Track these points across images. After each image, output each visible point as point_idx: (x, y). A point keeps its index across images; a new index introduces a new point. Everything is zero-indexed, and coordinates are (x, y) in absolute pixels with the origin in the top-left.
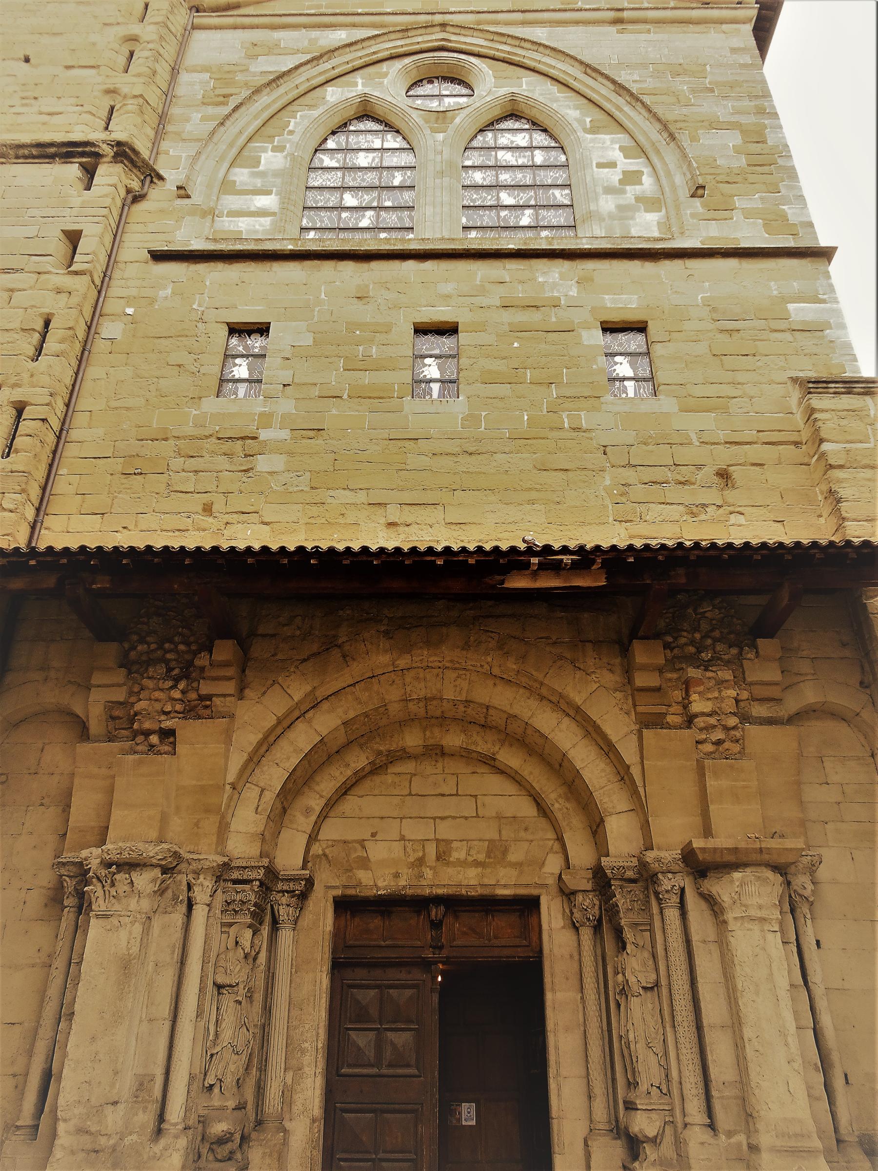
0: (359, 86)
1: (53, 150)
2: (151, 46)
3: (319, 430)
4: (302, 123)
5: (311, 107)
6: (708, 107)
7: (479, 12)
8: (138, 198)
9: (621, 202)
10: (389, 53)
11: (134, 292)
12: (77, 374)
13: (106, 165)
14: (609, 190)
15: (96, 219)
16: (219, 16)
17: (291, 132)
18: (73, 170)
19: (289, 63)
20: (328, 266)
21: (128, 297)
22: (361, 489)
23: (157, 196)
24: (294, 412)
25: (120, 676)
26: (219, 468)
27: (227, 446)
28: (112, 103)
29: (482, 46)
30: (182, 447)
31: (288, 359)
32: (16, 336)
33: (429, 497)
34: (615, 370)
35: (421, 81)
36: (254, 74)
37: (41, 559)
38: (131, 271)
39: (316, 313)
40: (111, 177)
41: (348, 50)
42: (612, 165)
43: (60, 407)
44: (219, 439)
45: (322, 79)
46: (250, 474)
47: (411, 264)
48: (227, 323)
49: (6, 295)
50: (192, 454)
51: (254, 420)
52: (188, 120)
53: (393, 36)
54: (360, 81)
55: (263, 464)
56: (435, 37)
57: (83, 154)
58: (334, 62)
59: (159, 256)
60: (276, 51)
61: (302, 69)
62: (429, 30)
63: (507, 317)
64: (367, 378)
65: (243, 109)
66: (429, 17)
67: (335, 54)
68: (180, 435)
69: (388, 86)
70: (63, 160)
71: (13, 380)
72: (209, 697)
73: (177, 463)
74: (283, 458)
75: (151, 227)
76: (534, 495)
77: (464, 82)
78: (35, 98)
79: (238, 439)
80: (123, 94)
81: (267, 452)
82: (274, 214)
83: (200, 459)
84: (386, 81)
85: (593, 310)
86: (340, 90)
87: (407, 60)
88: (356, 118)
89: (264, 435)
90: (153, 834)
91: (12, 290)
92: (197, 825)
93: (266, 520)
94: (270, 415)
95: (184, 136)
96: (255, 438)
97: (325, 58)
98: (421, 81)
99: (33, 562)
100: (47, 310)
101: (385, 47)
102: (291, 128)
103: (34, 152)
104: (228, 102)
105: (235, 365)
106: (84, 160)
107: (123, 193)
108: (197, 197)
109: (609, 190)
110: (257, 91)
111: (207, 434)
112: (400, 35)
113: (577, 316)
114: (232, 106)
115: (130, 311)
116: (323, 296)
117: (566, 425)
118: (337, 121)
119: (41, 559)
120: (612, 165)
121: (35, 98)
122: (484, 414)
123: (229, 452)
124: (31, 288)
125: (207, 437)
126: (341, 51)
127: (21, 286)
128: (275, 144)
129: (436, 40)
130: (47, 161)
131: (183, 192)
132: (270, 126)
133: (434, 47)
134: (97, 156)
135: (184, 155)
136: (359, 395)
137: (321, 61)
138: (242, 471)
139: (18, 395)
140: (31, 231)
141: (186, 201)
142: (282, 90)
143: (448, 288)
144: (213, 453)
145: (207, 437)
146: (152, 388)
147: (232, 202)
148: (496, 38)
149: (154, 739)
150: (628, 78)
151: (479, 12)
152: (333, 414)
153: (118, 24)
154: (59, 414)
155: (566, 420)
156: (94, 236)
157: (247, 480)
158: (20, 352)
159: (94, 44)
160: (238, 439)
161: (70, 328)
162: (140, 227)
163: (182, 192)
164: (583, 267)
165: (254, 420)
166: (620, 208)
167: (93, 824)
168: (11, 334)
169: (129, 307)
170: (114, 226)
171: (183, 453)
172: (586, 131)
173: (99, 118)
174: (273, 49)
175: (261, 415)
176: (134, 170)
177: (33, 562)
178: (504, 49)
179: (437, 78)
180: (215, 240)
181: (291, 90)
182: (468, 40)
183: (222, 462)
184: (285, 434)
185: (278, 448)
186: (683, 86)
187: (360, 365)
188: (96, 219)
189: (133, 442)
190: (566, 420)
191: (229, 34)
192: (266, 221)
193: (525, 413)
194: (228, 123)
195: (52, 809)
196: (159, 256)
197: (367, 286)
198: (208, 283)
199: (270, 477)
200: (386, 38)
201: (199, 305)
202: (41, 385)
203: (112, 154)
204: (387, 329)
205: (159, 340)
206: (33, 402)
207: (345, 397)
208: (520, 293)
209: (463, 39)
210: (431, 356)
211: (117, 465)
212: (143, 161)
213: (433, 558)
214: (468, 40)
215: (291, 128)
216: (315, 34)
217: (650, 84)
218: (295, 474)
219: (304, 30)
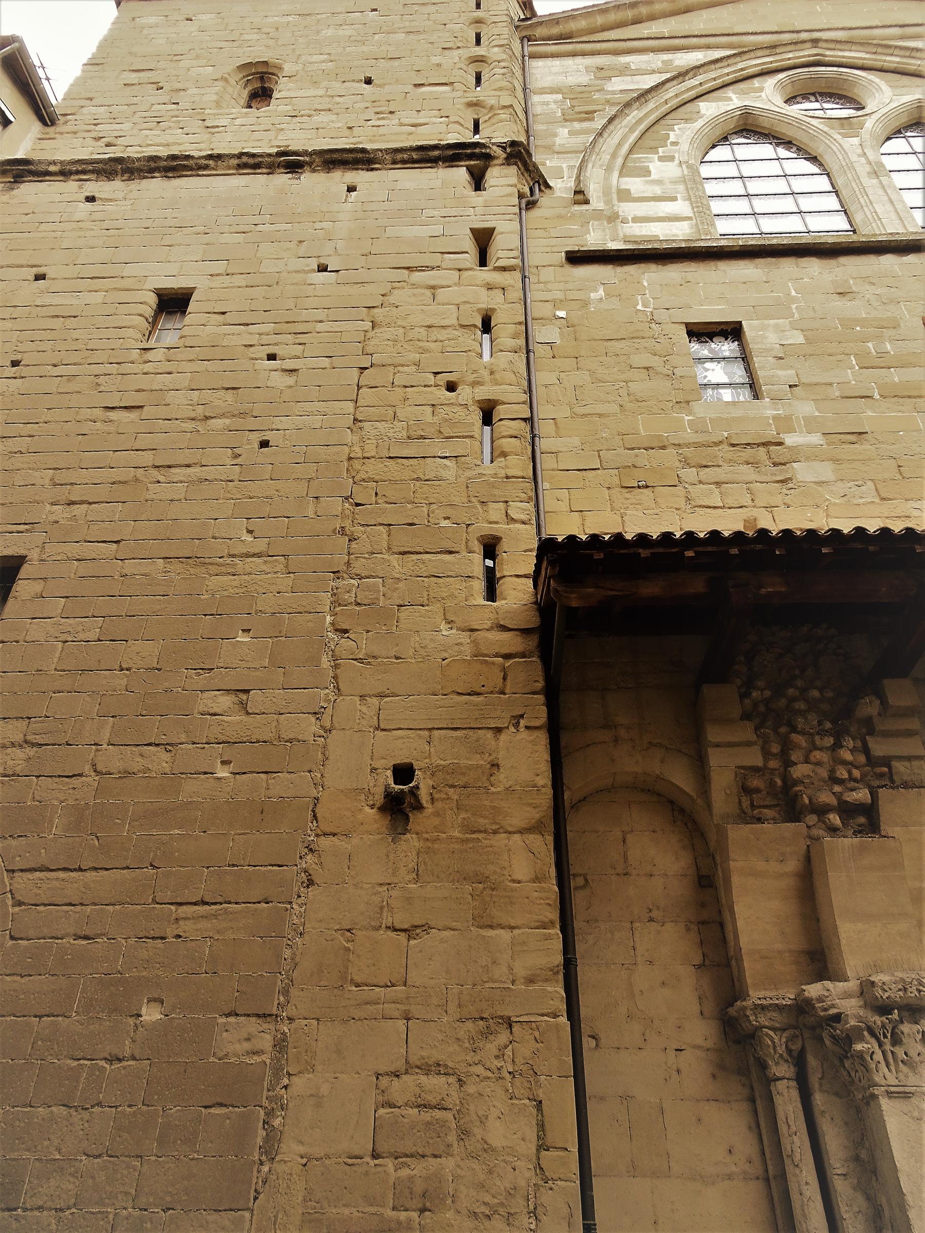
0: (735, 100)
1: (436, 153)
2: (503, 64)
3: (860, 433)
4: (683, 135)
7: (850, 29)
8: (531, 205)
10: (760, 68)
11: (559, 295)
13: (497, 167)
15: (508, 217)
16: (556, 44)
17: (675, 144)
18: (460, 174)
19: (648, 82)
20: (788, 265)
21: (554, 301)
24: (817, 414)
25: (746, 732)
26: (747, 479)
27: (748, 453)
28: (476, 117)
29: (864, 59)
30: (689, 455)
31: (781, 358)
35: (795, 97)
36: (614, 92)
37: (701, 549)
38: (547, 274)
39: (794, 311)
40: (503, 180)
41: (713, 67)
44: (733, 445)
45: (693, 93)
46: (790, 485)
47: (889, 260)
48: (687, 325)
49: (428, 293)
50: (705, 463)
52: (555, 135)
53: (760, 53)
54: (733, 96)
56: (807, 53)
57: (471, 157)
58: (700, 79)
59: (576, 258)
62: (799, 46)
64: (895, 376)
65: (616, 121)
66: (795, 36)
67: (701, 71)
68: (681, 442)
69: (767, 97)
70: (447, 164)
71: (471, 378)
72: (886, 761)
73: (689, 474)
75: (554, 233)
77: (845, 97)
78: (391, 113)
79: (758, 445)
80: (489, 106)
81: (802, 460)
82: (689, 218)
83: (716, 469)
84: (763, 94)
86: (714, 104)
88: (735, 133)
89: (790, 440)
94: (788, 418)
95: (557, 148)
97: (691, 74)
98: (795, 97)
99: (690, 554)
100: (484, 306)
101: (753, 64)
103: (415, 156)
105: (707, 370)
106: (472, 163)
108: (597, 203)
110: (628, 105)
111: (715, 440)
112: (767, 52)
116: (793, 293)
118: (718, 133)
119: (701, 549)
121: (391, 113)
123: (751, 460)
124: (455, 284)
125: (717, 444)
126: (706, 68)
127: (444, 283)
128: (661, 154)
129: (809, 56)
130: (429, 165)
132: (650, 137)
133: (808, 61)
134: (488, 158)
135: (564, 166)
137: (687, 78)
138: (778, 482)
139: (485, 392)
140: (438, 230)
141: (585, 207)
142: (651, 105)
145: (717, 444)
146: (623, 392)
147: (628, 209)
148: (879, 50)
149: (835, 819)
151: (850, 29)
152: (869, 416)
153: (459, 48)
156: (512, 232)
157: (788, 492)
158: (467, 349)
159: (439, 65)
160: (758, 445)
162: (540, 233)
163: (580, 197)
167: (778, 946)
168: (449, 330)
173: (468, 129)
176: (526, 175)
177: (690, 554)
178: (893, 60)
179: (814, 94)
181: (661, 105)
182: (847, 54)
183: (747, 472)
184: (816, 439)
188: (508, 217)
189: (621, 451)
191: (569, 62)
192: (685, 225)
194: (605, 135)
195: (669, 926)
196: (576, 258)
197: (847, 281)
198: (645, 284)
199: (820, 489)
200: (752, 55)
202: (509, 382)
203: (504, 155)
205: (610, 343)
206: (504, 400)
214: (847, 54)
216: (666, 57)
219: (652, 54)
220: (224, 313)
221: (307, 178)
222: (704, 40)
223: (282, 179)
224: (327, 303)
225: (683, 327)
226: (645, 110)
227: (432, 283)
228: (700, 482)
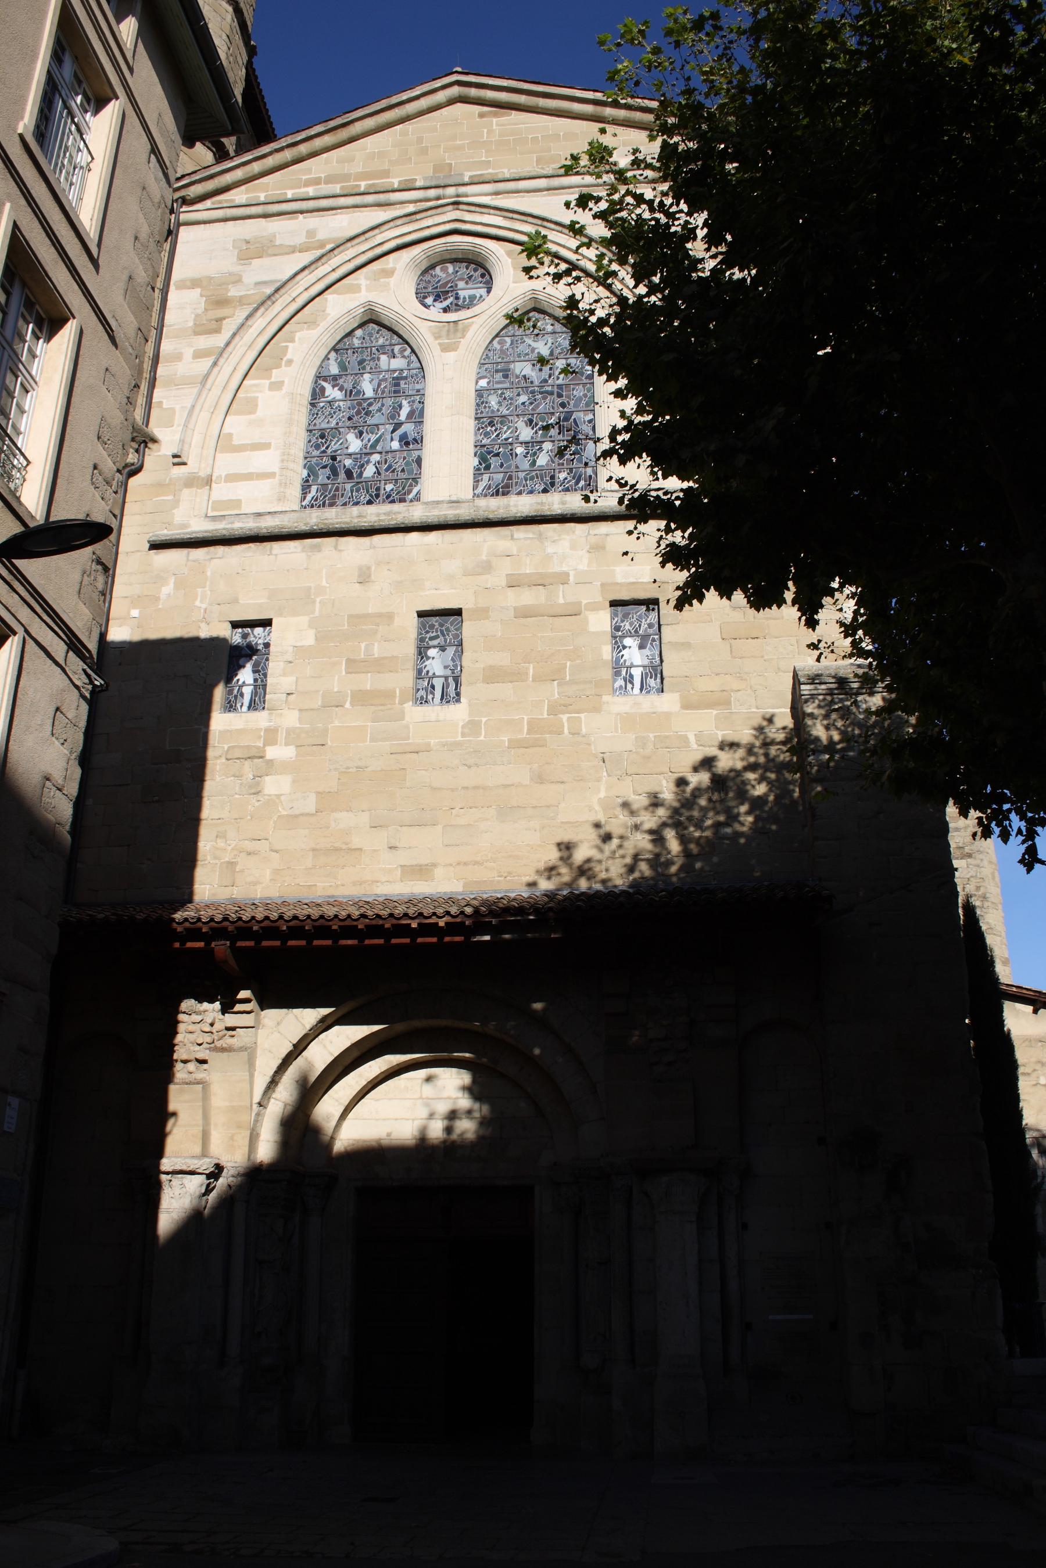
5: (312, 324)
24: (298, 725)
31: (290, 662)
41: (349, 244)
47: (414, 536)
51: (260, 737)
60: (270, 252)
61: (299, 277)
87: (416, 250)
90: (198, 1150)
92: (232, 1138)
93: (277, 848)
102: (289, 356)
104: (220, 328)
108: (195, 465)
114: (226, 335)
115: (135, 613)
117: (566, 731)
122: (484, 720)
126: (342, 248)
128: (273, 380)
136: (362, 698)
155: (566, 725)
163: (176, 460)
164: (596, 532)
165: (260, 737)
169: (134, 608)
175: (267, 730)
180: (214, 518)
185: (286, 767)
196: (157, 546)
201: (201, 602)
204: (390, 617)
209: (478, 218)
210: (434, 647)
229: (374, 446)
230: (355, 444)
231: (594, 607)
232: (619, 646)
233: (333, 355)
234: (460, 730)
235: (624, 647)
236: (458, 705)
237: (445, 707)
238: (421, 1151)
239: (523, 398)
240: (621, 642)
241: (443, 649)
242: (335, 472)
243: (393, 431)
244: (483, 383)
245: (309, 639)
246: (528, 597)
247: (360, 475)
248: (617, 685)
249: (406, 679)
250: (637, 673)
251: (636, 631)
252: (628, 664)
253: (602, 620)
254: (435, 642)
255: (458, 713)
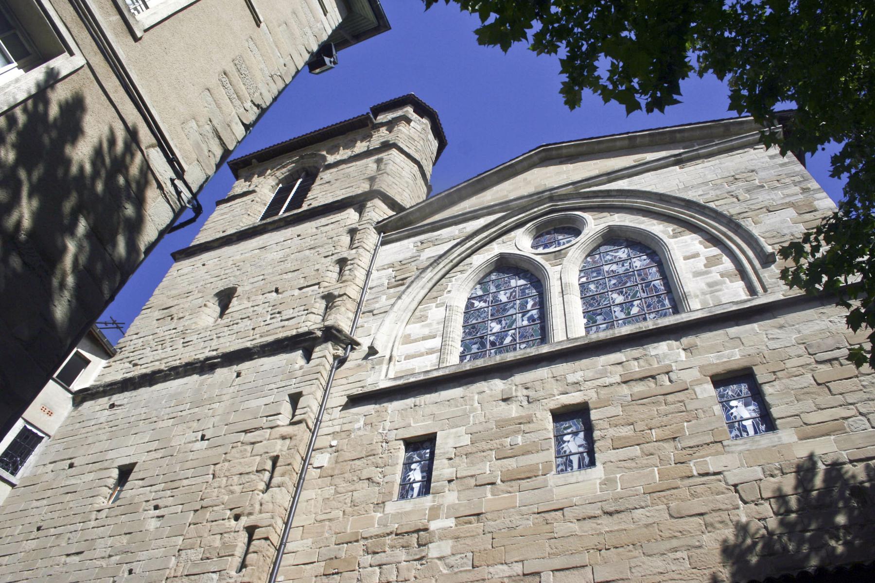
0: (497, 249)
6: (764, 198)
9: (710, 280)
12: (294, 498)
14: (697, 274)
18: (298, 356)
22: (516, 562)
23: (356, 357)
27: (402, 541)
30: (369, 545)
31: (451, 459)
32: (253, 476)
33: (576, 561)
34: (732, 414)
42: (696, 255)
43: (280, 526)
46: (424, 562)
55: (434, 551)
56: (546, 206)
63: (625, 390)
64: (511, 464)
74: (450, 542)
75: (351, 380)
76: (675, 543)
83: (383, 554)
85: (702, 368)
89: (434, 526)
91: (253, 443)
94: (439, 507)
96: (426, 530)
100: (275, 454)
102: (449, 289)
107: (331, 359)
109: (697, 274)
113: (687, 377)
120: (696, 255)
122: (618, 476)
125: (388, 534)
131: (372, 351)
140: (271, 399)
143: (578, 376)
144: (392, 547)
146: (348, 501)
150: (694, 194)
154: (279, 532)
155: (694, 468)
159: (318, 270)
161: (289, 464)
162: (344, 381)
164: (823, 311)
166: (710, 285)
170: (324, 384)
171: (370, 551)
172: (670, 237)
174: (435, 243)
183: (402, 555)
184: (451, 522)
185: (444, 535)
186: (739, 188)
187: (509, 453)
189: (333, 546)
190: (694, 468)
193: (656, 469)
194: (404, 297)
201: (384, 429)
207: (499, 481)
208: (635, 368)
210: (569, 434)
211: (320, 568)
212: (346, 336)
213: (19, 425)
215: (449, 289)
217: (712, 194)
218: (459, 556)
220: (143, 479)
221: (219, 371)
222: (489, 210)
223: (194, 379)
224: (195, 464)
225: (402, 442)
226: (437, 270)
227: (253, 440)
228: (371, 566)
229: (510, 326)
230: (496, 327)
231: (699, 382)
232: (727, 408)
233: (478, 286)
234: (598, 486)
235: (732, 408)
236: (593, 469)
237: (583, 472)
238: (125, 239)
239: (613, 281)
240: (728, 405)
241: (575, 434)
242: (483, 345)
243: (523, 316)
244: (584, 280)
245: (466, 440)
246: (639, 388)
247: (502, 343)
248: (733, 434)
249: (551, 454)
250: (748, 424)
251: (739, 395)
252: (738, 418)
253: (708, 390)
254: (569, 431)
255: (597, 473)
